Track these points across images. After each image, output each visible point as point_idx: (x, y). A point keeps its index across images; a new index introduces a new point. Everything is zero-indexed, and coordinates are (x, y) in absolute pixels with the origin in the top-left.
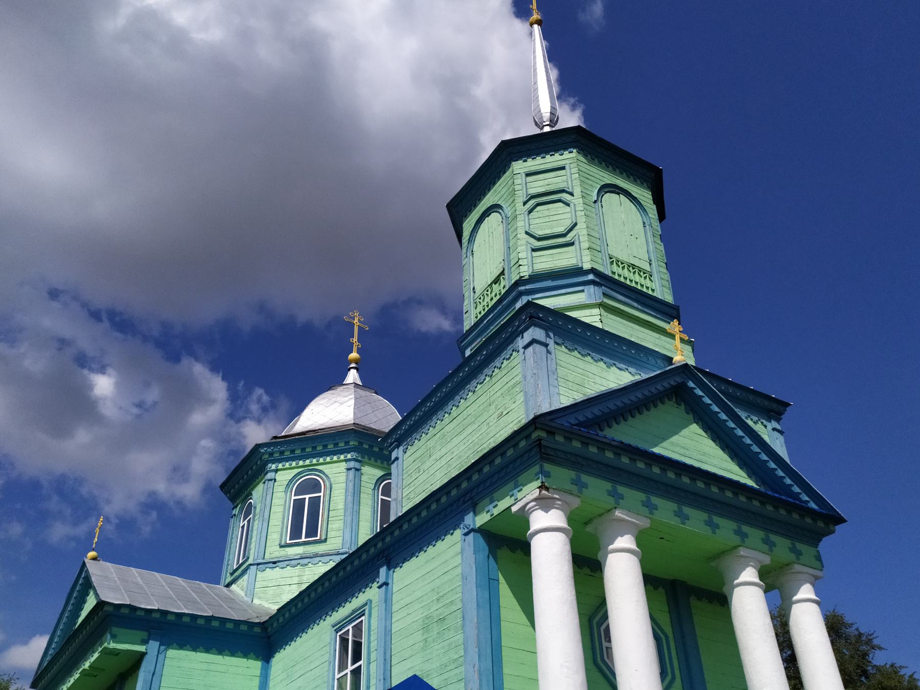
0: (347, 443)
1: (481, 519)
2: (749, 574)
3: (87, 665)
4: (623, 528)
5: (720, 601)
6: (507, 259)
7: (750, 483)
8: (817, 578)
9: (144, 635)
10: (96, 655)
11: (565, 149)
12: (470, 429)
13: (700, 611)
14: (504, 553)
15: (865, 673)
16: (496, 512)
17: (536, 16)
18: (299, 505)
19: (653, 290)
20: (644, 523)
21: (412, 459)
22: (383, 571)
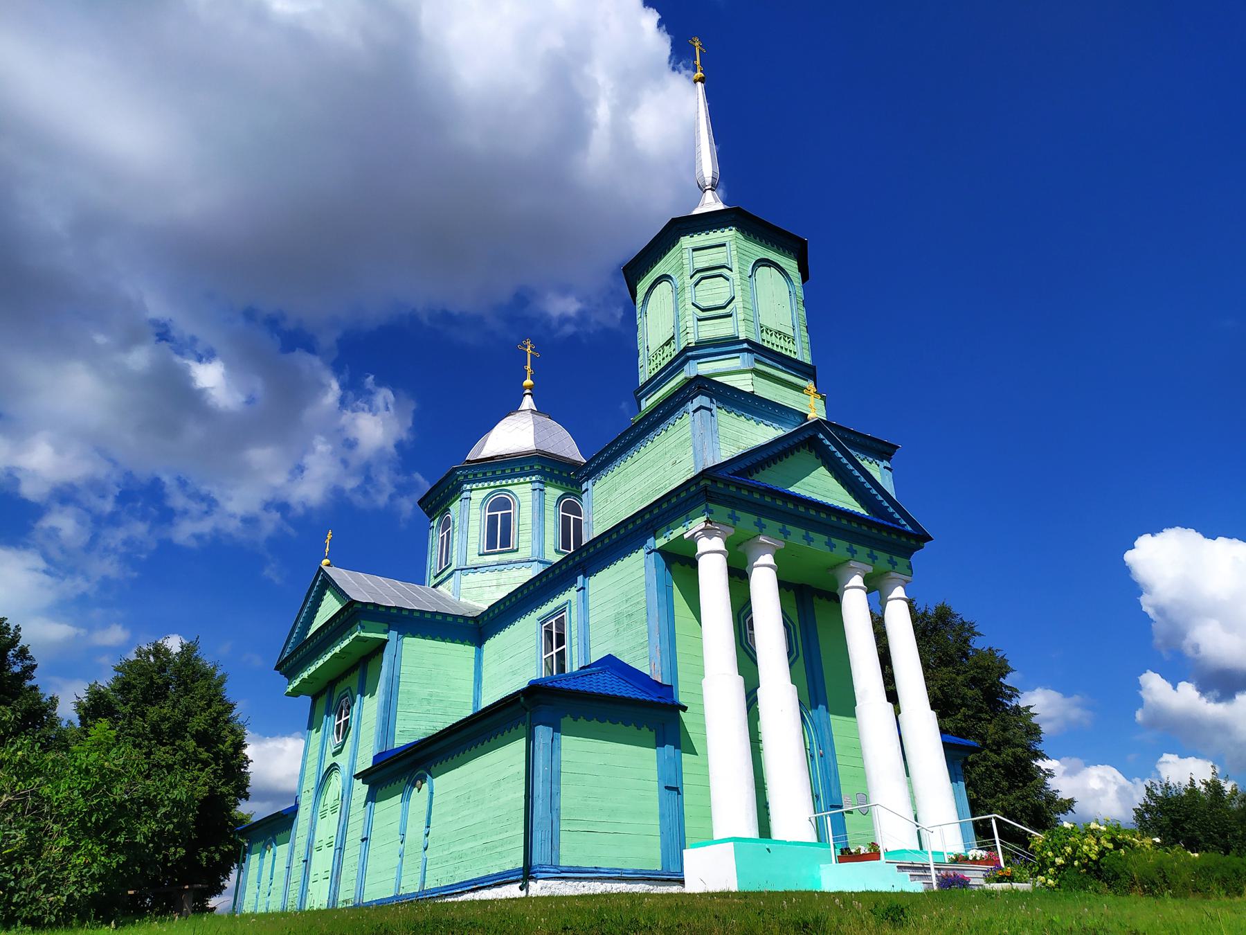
0: (532, 467)
1: (661, 542)
2: (857, 580)
3: (337, 649)
4: (765, 549)
5: (834, 598)
6: (676, 326)
7: (862, 511)
8: (907, 582)
9: (386, 626)
10: (346, 642)
11: (726, 227)
12: (649, 472)
13: (820, 605)
14: (676, 566)
15: (965, 655)
16: (672, 537)
17: (699, 74)
18: (492, 521)
20: (781, 545)
21: (600, 491)
22: (580, 578)
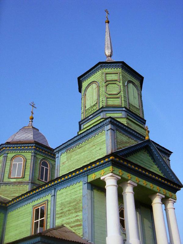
19: (139, 115)
